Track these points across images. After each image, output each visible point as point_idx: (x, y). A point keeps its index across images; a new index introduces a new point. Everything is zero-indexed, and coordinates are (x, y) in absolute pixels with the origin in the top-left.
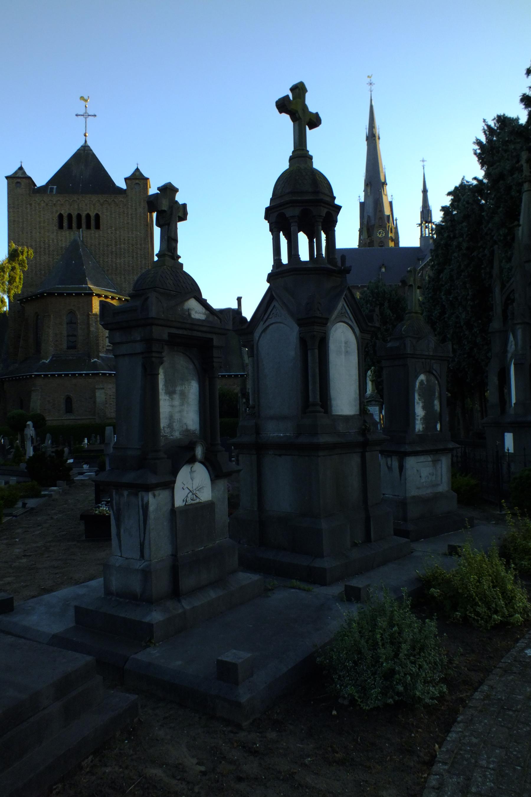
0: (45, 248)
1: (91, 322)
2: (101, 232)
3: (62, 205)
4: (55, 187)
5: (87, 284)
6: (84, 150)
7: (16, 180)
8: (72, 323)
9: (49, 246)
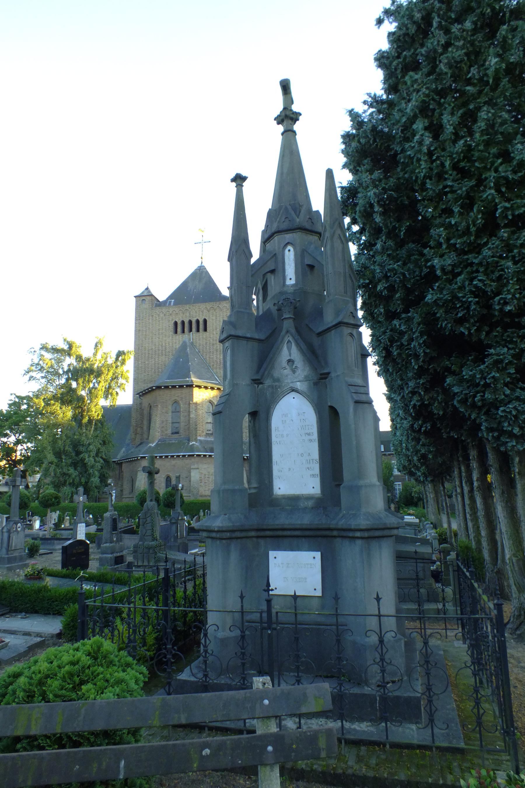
0: (162, 350)
1: (191, 410)
2: (208, 334)
3: (177, 314)
4: (173, 300)
5: (190, 377)
6: (200, 270)
7: (142, 298)
8: (176, 411)
9: (166, 349)
